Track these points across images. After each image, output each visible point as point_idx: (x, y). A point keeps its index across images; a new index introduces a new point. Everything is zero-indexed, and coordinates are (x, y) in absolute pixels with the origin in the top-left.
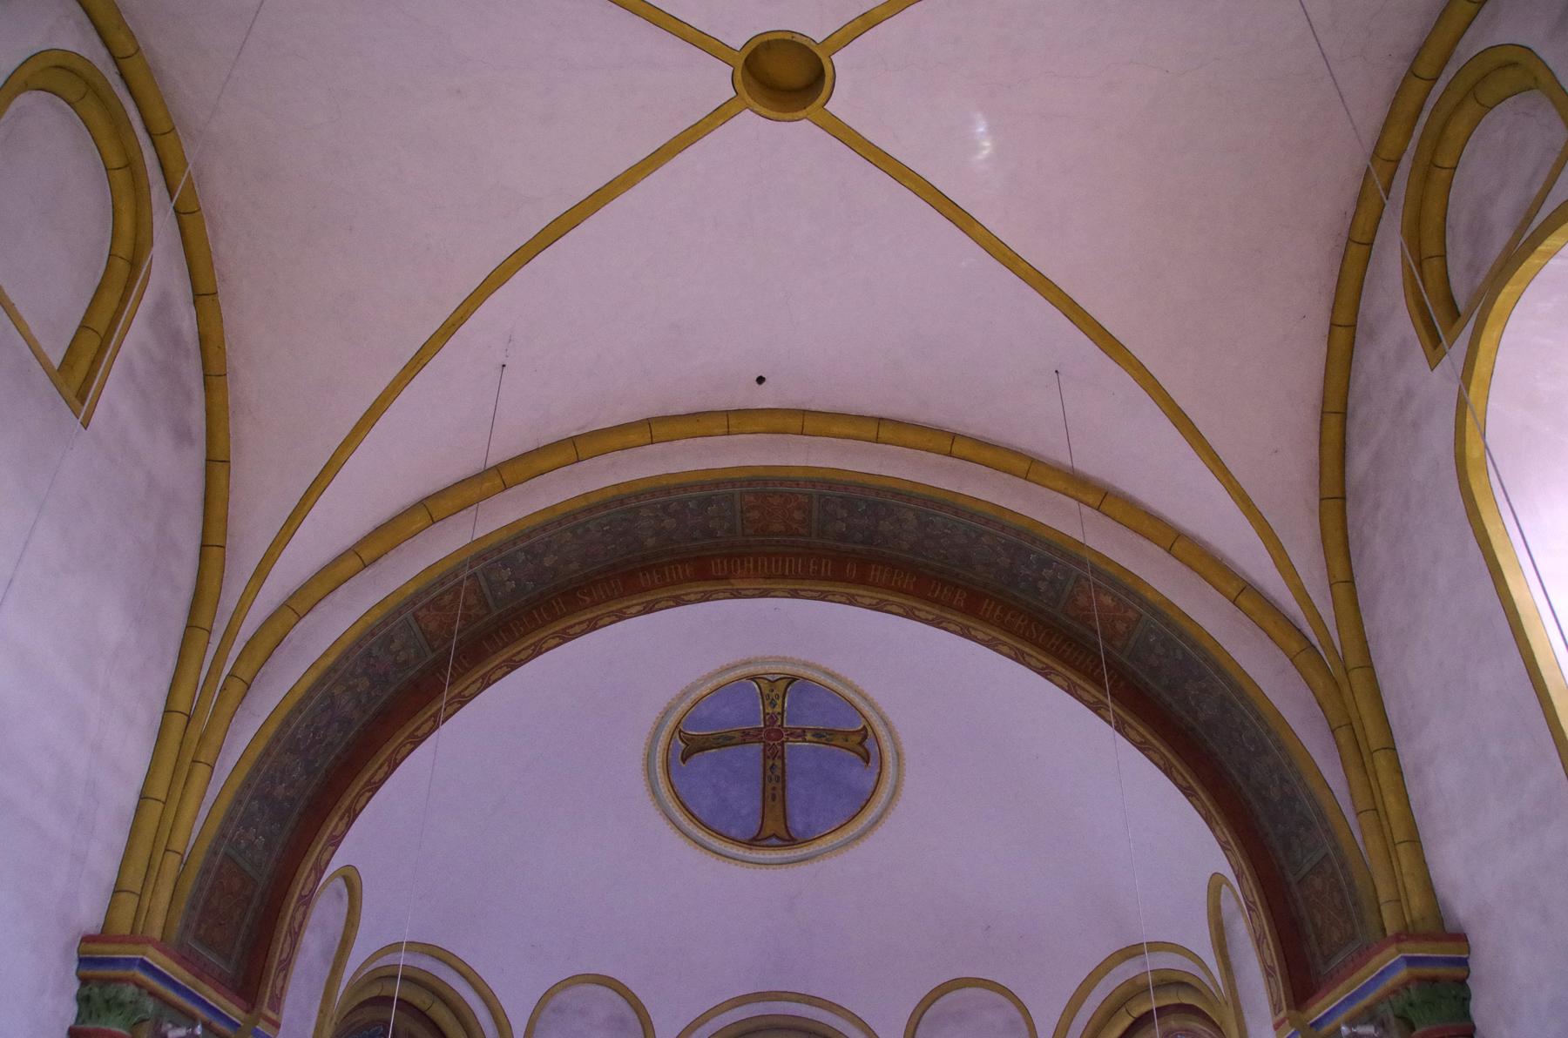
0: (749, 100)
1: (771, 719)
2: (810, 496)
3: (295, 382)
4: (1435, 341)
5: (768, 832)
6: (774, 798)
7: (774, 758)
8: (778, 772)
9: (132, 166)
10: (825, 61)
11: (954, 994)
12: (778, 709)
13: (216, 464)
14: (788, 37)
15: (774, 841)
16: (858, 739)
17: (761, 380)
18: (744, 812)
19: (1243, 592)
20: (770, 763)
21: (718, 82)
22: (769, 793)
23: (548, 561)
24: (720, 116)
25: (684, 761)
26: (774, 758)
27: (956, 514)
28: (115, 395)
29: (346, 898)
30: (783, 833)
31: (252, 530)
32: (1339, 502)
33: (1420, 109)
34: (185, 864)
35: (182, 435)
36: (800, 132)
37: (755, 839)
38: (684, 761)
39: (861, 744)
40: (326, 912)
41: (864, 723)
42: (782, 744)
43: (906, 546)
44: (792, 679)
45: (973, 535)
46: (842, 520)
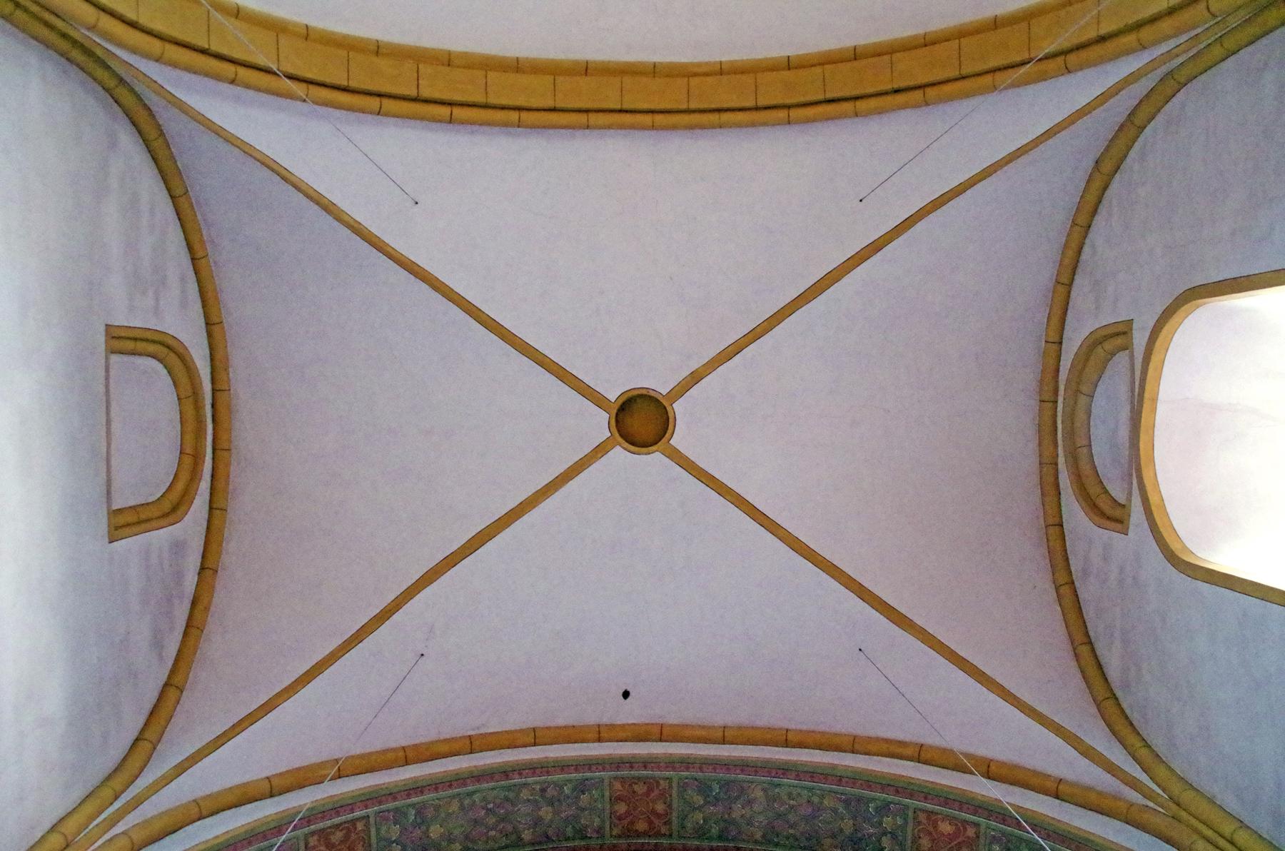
0: (620, 440)
2: (669, 779)
3: (260, 630)
4: (1120, 521)
9: (197, 458)
10: (669, 409)
13: (173, 687)
14: (644, 392)
17: (626, 695)
19: (1056, 790)
21: (599, 425)
24: (600, 451)
28: (130, 545)
32: (1055, 347)
33: (1055, 422)
35: (157, 644)
36: (655, 460)
43: (758, 836)
46: (700, 808)
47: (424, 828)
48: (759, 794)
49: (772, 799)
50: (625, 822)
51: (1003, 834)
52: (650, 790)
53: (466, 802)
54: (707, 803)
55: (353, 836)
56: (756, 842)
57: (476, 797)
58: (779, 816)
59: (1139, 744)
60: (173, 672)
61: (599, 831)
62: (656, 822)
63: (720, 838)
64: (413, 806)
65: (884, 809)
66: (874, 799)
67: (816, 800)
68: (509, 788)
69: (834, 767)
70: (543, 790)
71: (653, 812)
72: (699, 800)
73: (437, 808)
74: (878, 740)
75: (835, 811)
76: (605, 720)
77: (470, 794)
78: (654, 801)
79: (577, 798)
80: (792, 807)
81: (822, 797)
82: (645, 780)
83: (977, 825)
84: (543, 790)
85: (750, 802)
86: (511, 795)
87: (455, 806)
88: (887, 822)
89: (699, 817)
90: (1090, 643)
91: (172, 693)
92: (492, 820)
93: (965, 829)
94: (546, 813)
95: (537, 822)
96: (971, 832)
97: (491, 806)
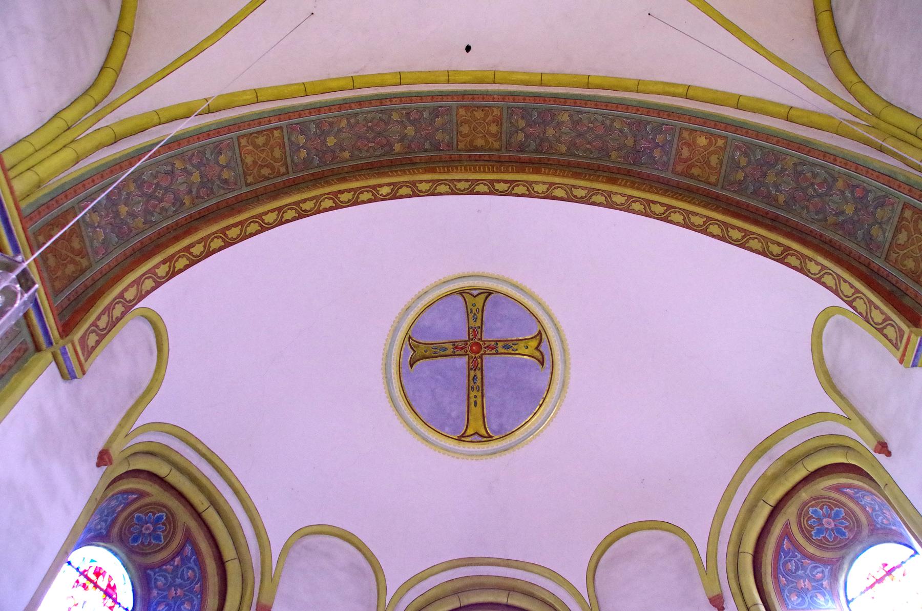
1: (474, 332)
5: (470, 432)
6: (476, 403)
7: (476, 366)
8: (479, 383)
11: (624, 540)
12: (478, 324)
15: (477, 438)
16: (534, 343)
17: (468, 49)
18: (454, 414)
20: (472, 373)
22: (472, 400)
23: (331, 141)
25: (411, 366)
26: (476, 366)
27: (596, 107)
29: (155, 353)
30: (483, 432)
31: (146, 56)
34: (39, 186)
37: (462, 436)
38: (411, 366)
39: (537, 348)
40: (131, 337)
41: (539, 328)
42: (481, 358)
44: (489, 293)
45: (608, 122)
47: (322, 138)
48: (565, 117)
49: (576, 123)
50: (468, 139)
51: (744, 143)
52: (486, 116)
53: (352, 121)
54: (528, 125)
55: (272, 142)
56: (562, 154)
57: (360, 118)
58: (580, 135)
59: (854, 79)
60: (121, 18)
61: (449, 145)
62: (491, 140)
63: (536, 151)
64: (313, 121)
65: (658, 129)
66: (649, 123)
67: (608, 122)
68: (381, 112)
69: (625, 99)
70: (408, 114)
71: (489, 133)
72: (522, 124)
73: (331, 124)
74: (656, 83)
75: (621, 131)
76: (453, 68)
77: (356, 115)
78: (489, 124)
79: (433, 120)
80: (591, 128)
81: (613, 121)
82: (482, 108)
83: (726, 138)
84: (408, 114)
85: (559, 124)
86: (385, 117)
87: (344, 123)
88: (659, 139)
89: (521, 136)
90: (831, 10)
91: (124, 39)
92: (370, 135)
93: (716, 141)
94: (410, 131)
95: (403, 138)
96: (720, 142)
97: (370, 124)
